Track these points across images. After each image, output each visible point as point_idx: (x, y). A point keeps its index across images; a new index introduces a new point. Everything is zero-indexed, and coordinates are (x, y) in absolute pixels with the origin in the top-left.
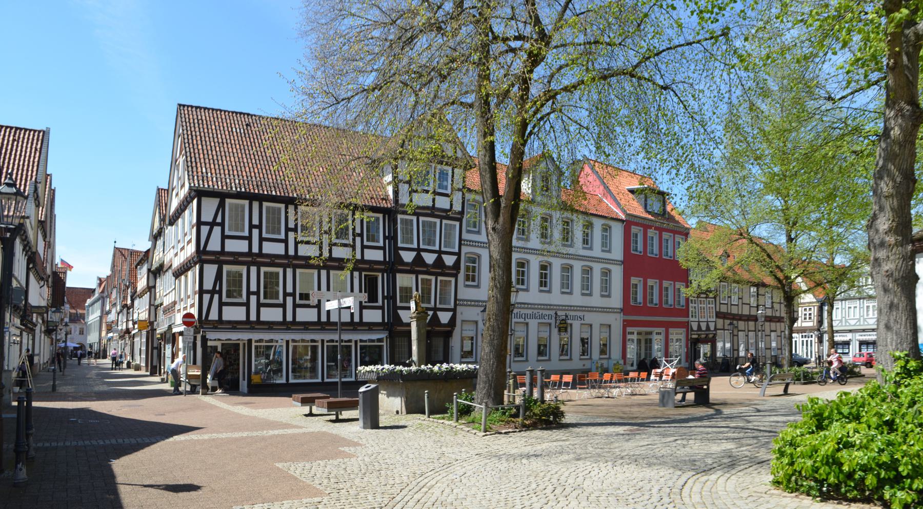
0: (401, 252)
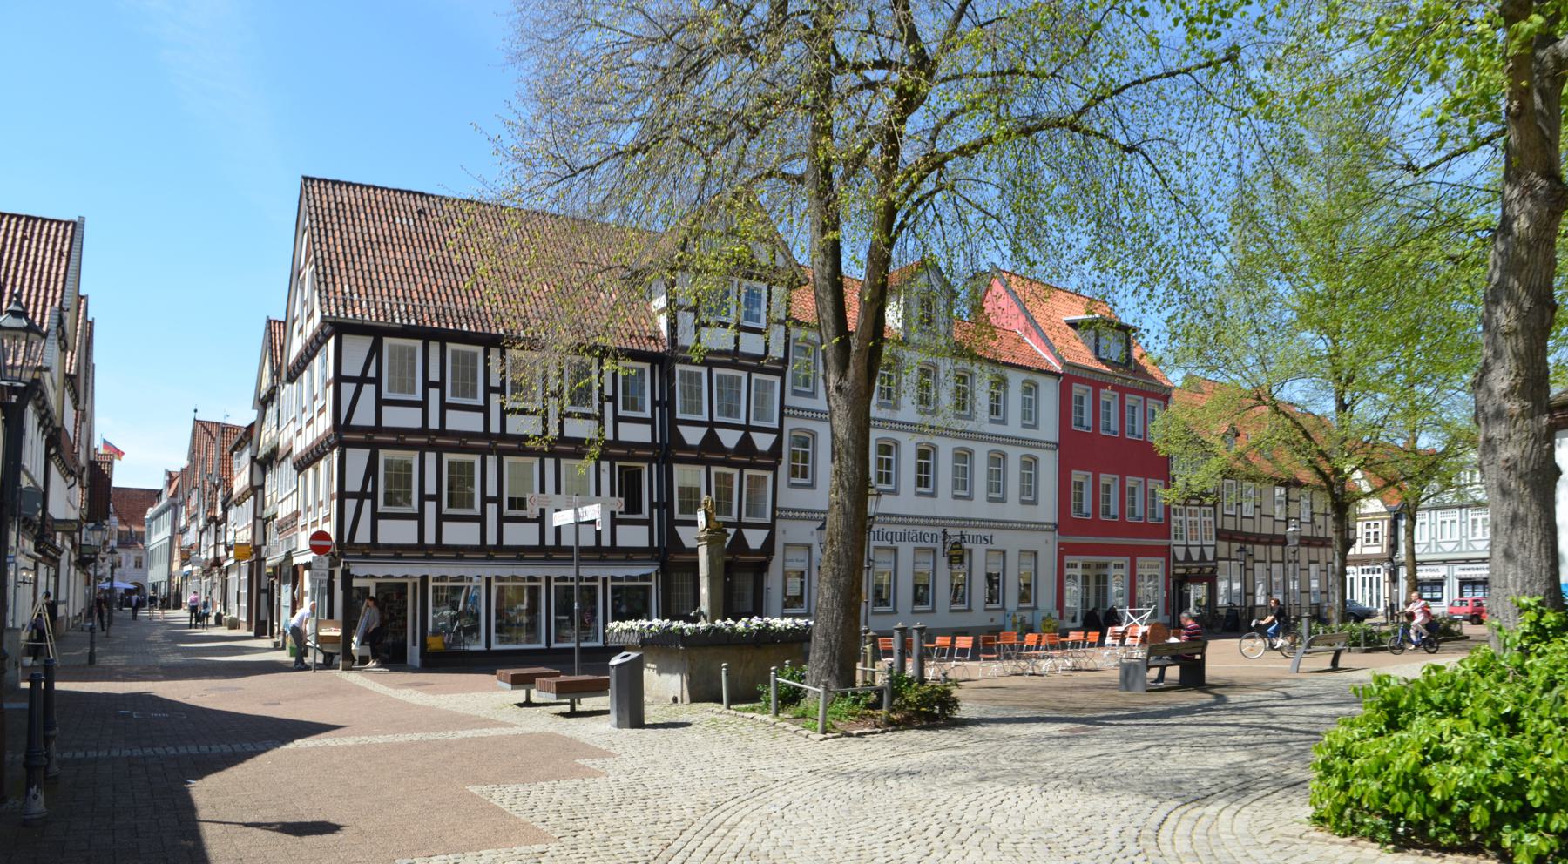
0: (682, 428)
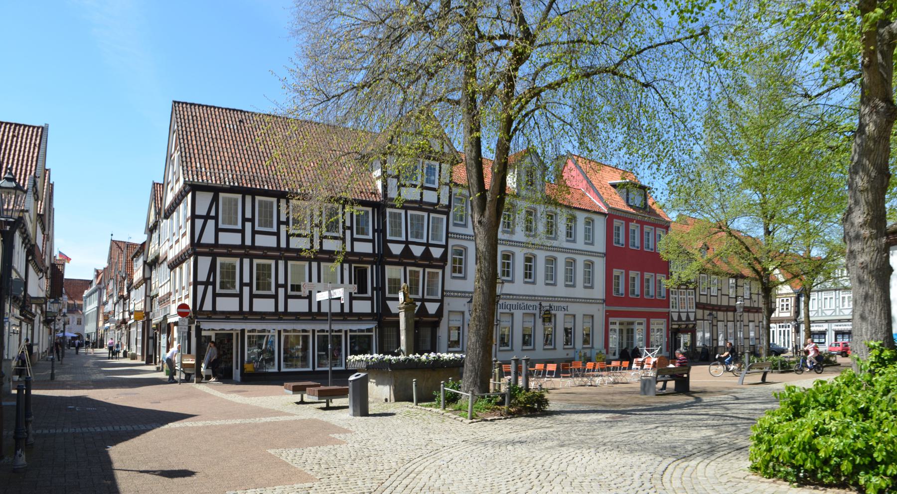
0: (390, 245)
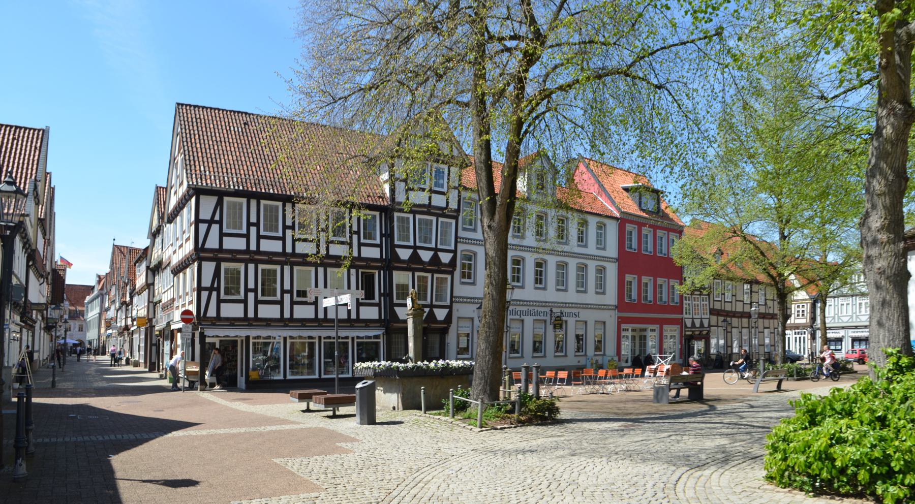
0: (398, 250)
